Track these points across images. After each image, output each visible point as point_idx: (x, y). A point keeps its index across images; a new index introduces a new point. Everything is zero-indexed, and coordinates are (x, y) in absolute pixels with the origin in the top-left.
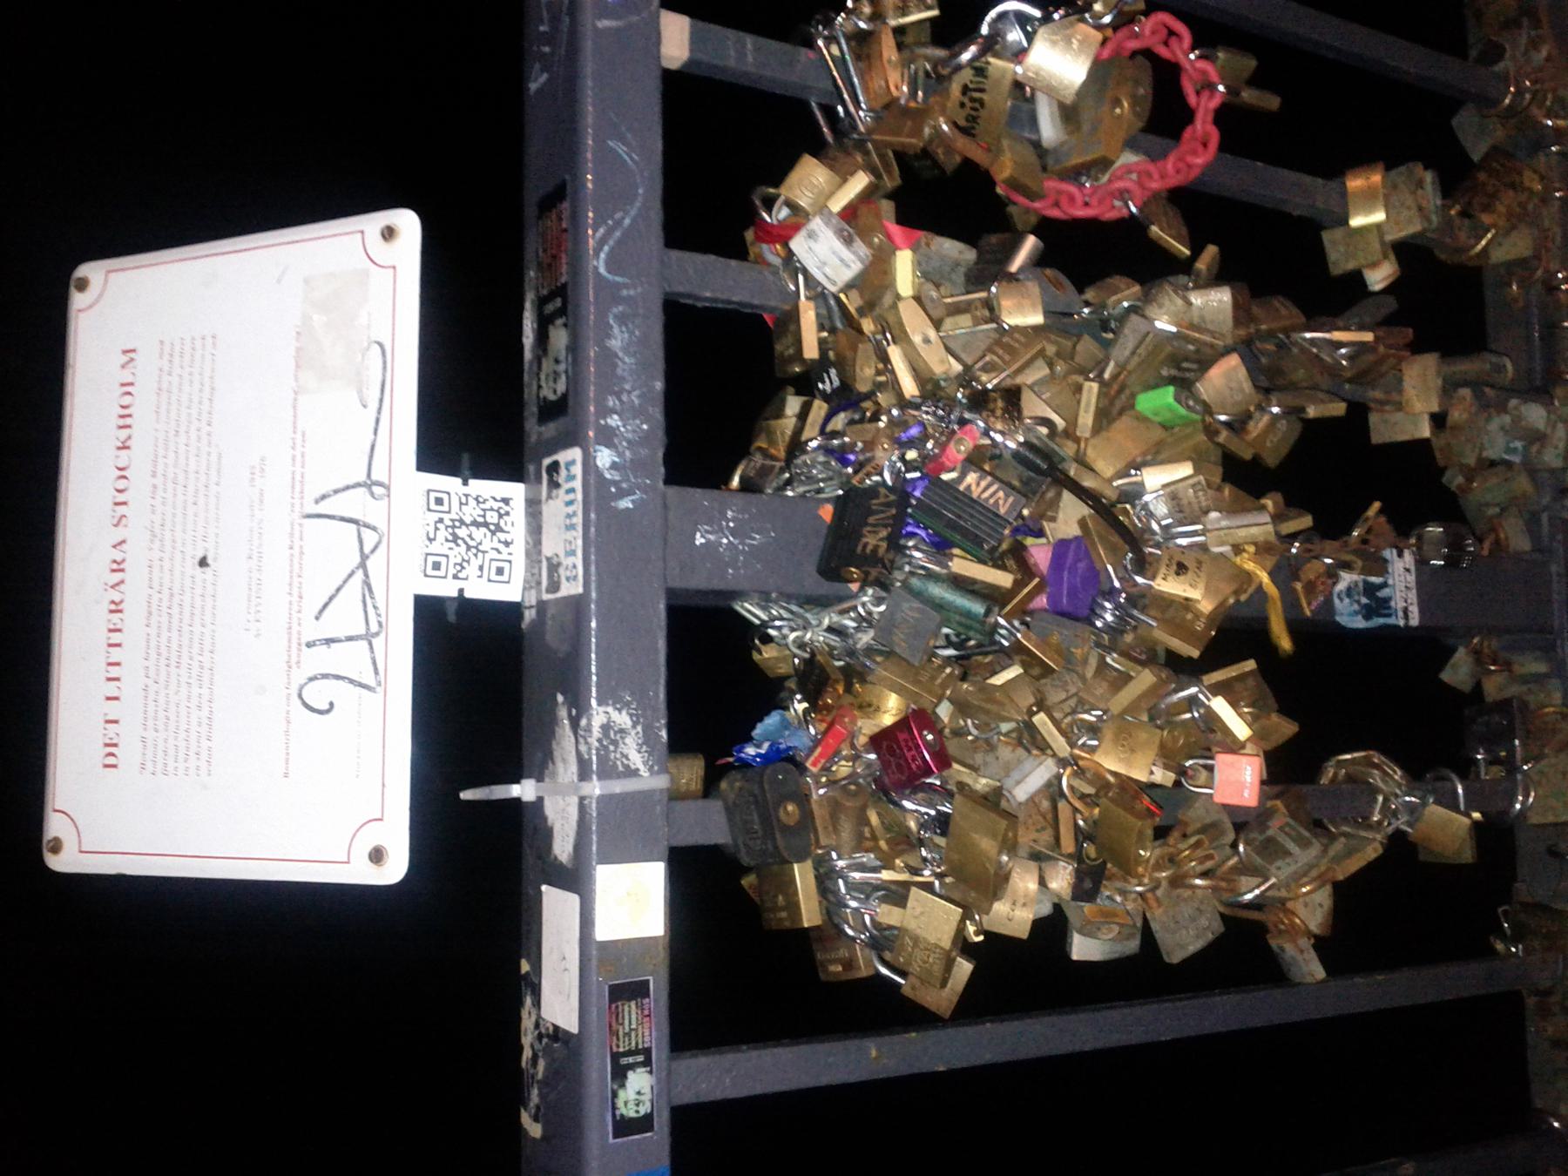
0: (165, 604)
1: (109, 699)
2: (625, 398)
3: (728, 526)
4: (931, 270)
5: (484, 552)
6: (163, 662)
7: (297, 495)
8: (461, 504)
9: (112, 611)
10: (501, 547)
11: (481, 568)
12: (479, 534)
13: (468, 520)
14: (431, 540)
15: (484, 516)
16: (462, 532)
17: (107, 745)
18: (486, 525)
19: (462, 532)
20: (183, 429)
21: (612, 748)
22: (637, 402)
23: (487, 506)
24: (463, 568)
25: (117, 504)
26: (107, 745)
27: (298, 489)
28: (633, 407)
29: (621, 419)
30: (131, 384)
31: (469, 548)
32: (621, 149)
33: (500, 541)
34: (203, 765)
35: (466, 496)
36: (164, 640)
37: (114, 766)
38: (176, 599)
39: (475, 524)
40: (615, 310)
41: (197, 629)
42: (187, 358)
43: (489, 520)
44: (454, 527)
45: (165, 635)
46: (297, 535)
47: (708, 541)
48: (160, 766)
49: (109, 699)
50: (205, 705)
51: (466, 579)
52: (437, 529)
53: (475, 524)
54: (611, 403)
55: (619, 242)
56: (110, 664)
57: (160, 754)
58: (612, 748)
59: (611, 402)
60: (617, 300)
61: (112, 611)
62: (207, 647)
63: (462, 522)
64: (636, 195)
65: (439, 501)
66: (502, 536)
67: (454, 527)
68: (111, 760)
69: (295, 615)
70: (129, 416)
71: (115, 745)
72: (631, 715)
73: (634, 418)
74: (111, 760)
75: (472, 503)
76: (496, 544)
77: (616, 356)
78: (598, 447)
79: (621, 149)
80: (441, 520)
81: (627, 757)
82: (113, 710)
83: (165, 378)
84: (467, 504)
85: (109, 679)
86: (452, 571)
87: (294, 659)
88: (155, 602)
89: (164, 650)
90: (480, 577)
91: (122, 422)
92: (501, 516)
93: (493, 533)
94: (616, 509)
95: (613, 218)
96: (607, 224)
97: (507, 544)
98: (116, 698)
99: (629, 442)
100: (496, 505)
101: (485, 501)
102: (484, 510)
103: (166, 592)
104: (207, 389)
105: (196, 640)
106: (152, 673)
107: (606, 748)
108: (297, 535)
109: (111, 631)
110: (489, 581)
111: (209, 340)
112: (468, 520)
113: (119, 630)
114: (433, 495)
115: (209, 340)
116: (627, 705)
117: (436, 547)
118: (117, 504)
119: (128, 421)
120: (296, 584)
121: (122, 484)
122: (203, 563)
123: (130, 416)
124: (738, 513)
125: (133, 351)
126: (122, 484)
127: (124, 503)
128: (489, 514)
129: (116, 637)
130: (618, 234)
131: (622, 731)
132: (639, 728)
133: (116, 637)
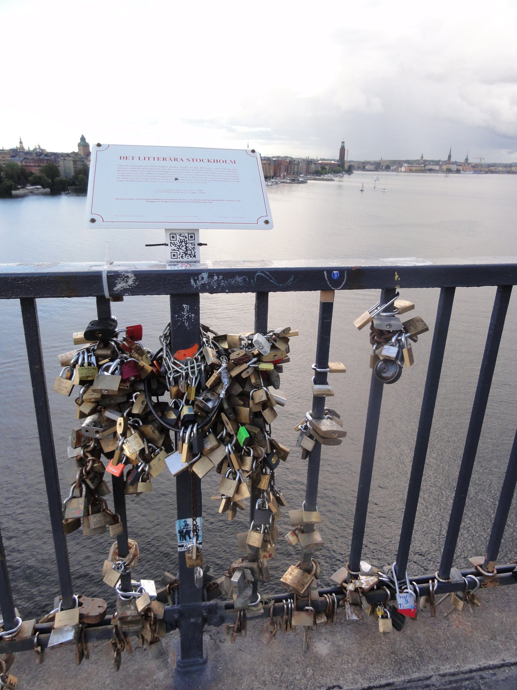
0: (165, 170)
1: (139, 157)
2: (223, 281)
3: (189, 315)
4: (353, 581)
5: (179, 251)
6: (149, 170)
7: (194, 201)
8: (192, 243)
9: (163, 158)
10: (181, 255)
11: (174, 250)
12: (184, 248)
13: (187, 245)
14: (180, 235)
15: (189, 250)
16: (183, 244)
17: (126, 157)
18: (187, 250)
19: (183, 244)
20: (213, 174)
21: (122, 279)
22: (222, 285)
23: (192, 251)
24: (173, 245)
25: (193, 159)
26: (126, 157)
27: (196, 201)
28: (220, 284)
29: (216, 280)
30: (226, 163)
31: (179, 246)
32: (292, 279)
33: (182, 255)
34: (119, 180)
35: (195, 245)
36: (155, 170)
37: (121, 159)
38: (167, 173)
39: (186, 247)
40: (247, 278)
41: (158, 178)
42: (233, 175)
43: (188, 251)
44: (185, 241)
45: (157, 170)
46: (184, 201)
47: (184, 309)
48: (120, 169)
49: (139, 157)
50: (137, 180)
51: (171, 246)
52: (183, 236)
53: (186, 247)
54: (220, 277)
55: (266, 278)
56: (149, 158)
57: (123, 170)
58: (122, 279)
59: (221, 277)
60: (250, 278)
61: (163, 158)
62: (153, 180)
63: (186, 244)
64: (279, 284)
65: (191, 237)
66: (184, 255)
67: (185, 241)
68: (122, 158)
69: (161, 201)
70: (217, 162)
71: (126, 159)
72: (132, 285)
73: (217, 284)
74: (122, 158)
75: (193, 247)
76: (181, 253)
77: (234, 279)
78: (208, 273)
79: (292, 279)
80: (186, 238)
81: (119, 283)
82: (136, 159)
83: (227, 170)
84: (192, 245)
85: (145, 158)
86: (172, 242)
87: (174, 201)
88: (166, 168)
89: (152, 170)
90: (172, 250)
91: (215, 160)
92: (190, 255)
93: (184, 253)
94: (191, 279)
95: (272, 277)
96: (270, 275)
97: (182, 257)
98: (139, 159)
99: (210, 282)
100: (193, 253)
101: (194, 250)
102: (191, 250)
103: (169, 171)
104: (225, 180)
105: (155, 178)
106: (146, 168)
107: (122, 277)
108: (184, 201)
109: (158, 158)
110: (171, 252)
111: (237, 180)
112: (187, 245)
113: (158, 160)
114: (193, 235)
115: (237, 180)
116: (135, 284)
117: (178, 236)
118: (193, 159)
119: (216, 162)
120: (169, 201)
121: (198, 160)
122: (176, 179)
123: (217, 162)
124: (194, 318)
125: (235, 163)
126: (198, 160)
127: (193, 161)
128: (190, 251)
129: (156, 159)
130: (268, 278)
131: (127, 282)
132: (128, 287)
133: (156, 159)
